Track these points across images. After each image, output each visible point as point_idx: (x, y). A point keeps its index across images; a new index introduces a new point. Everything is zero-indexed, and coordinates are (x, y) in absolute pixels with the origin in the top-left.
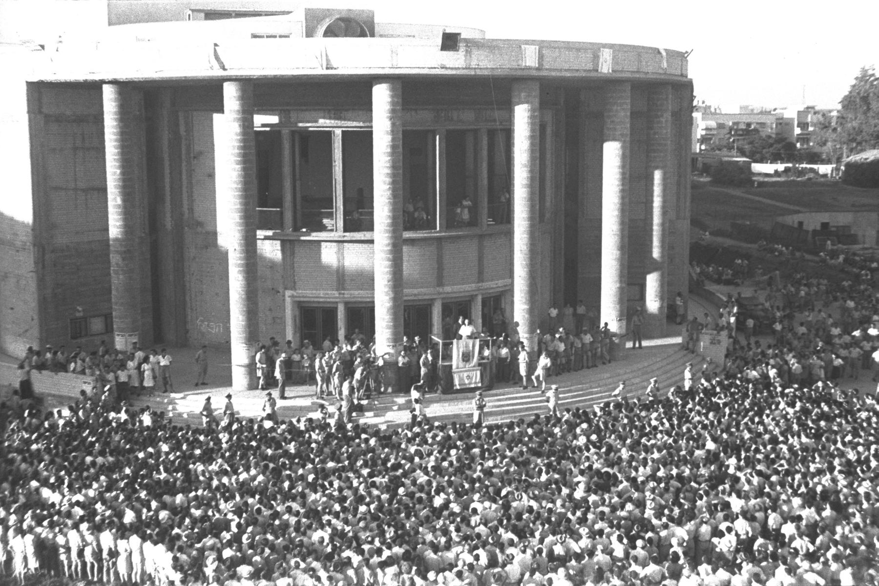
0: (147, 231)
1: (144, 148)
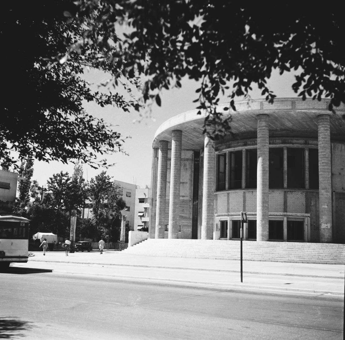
0: (192, 198)
1: (193, 170)
